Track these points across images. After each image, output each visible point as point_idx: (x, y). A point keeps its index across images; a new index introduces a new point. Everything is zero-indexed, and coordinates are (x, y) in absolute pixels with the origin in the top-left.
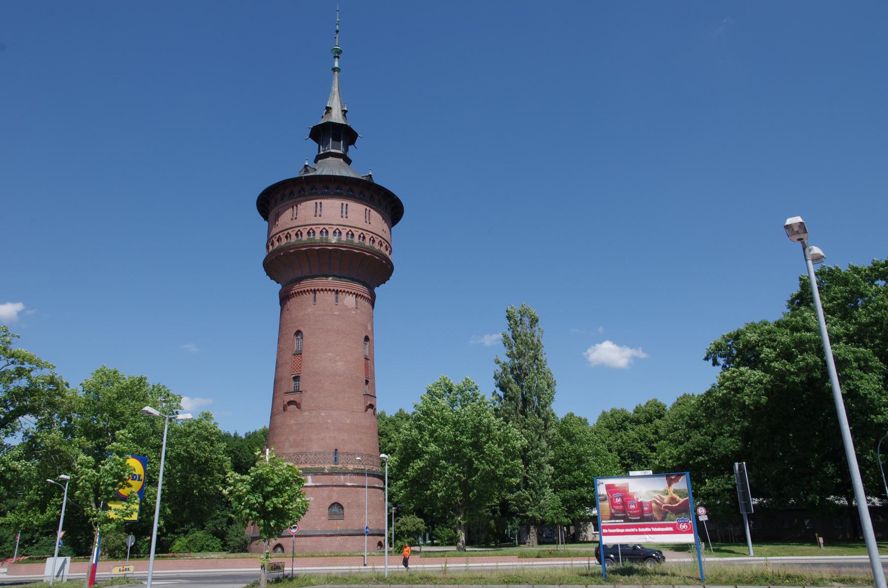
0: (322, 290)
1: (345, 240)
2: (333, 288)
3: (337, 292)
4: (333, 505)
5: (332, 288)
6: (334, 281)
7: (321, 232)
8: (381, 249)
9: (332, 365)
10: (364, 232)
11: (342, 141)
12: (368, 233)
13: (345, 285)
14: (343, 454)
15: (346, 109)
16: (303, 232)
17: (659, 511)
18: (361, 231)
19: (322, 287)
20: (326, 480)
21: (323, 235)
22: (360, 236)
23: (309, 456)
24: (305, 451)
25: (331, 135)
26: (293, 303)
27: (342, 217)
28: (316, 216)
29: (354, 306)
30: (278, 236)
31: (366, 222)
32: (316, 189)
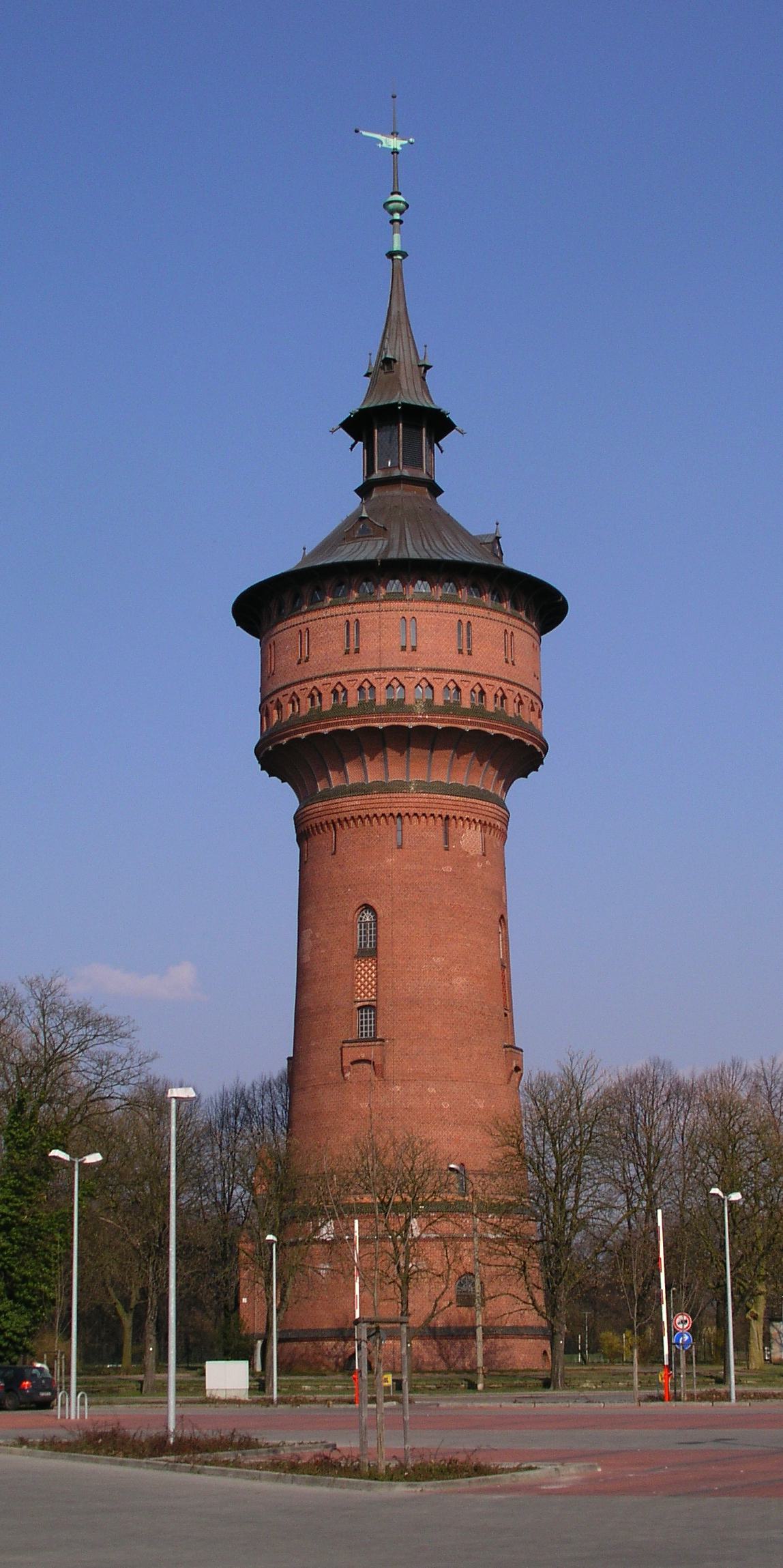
7: (361, 688)
12: (511, 687)
14: (475, 1174)
17: (141, 1299)
19: (400, 810)
26: (322, 841)
29: (480, 852)
31: (507, 662)
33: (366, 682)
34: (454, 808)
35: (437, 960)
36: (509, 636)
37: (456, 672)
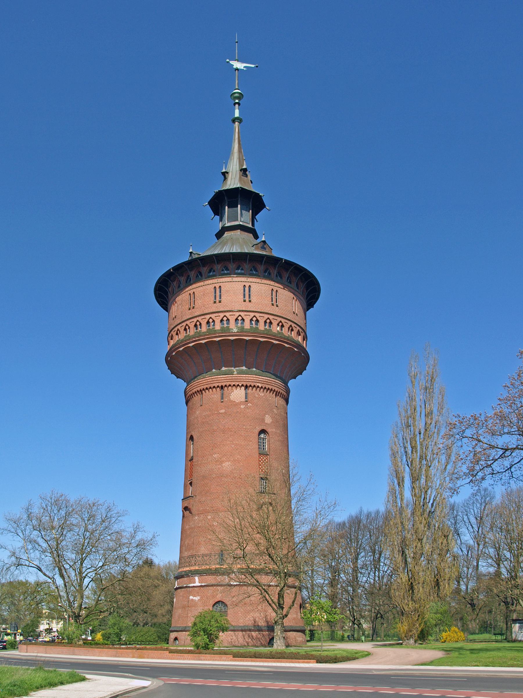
0: (210, 388)
1: (249, 328)
2: (217, 384)
3: (222, 387)
4: (218, 602)
5: (216, 385)
6: (239, 375)
7: (222, 321)
8: (293, 335)
9: (219, 466)
10: (271, 317)
11: (239, 206)
13: (231, 378)
15: (244, 167)
16: (201, 322)
18: (266, 316)
20: (211, 579)
21: (223, 324)
22: (265, 322)
23: (198, 559)
24: (194, 554)
25: (226, 204)
27: (245, 301)
28: (215, 302)
29: (243, 399)
30: (176, 329)
32: (214, 271)
33: (240, 317)
34: (225, 381)
35: (215, 456)
36: (275, 292)
37: (256, 312)
